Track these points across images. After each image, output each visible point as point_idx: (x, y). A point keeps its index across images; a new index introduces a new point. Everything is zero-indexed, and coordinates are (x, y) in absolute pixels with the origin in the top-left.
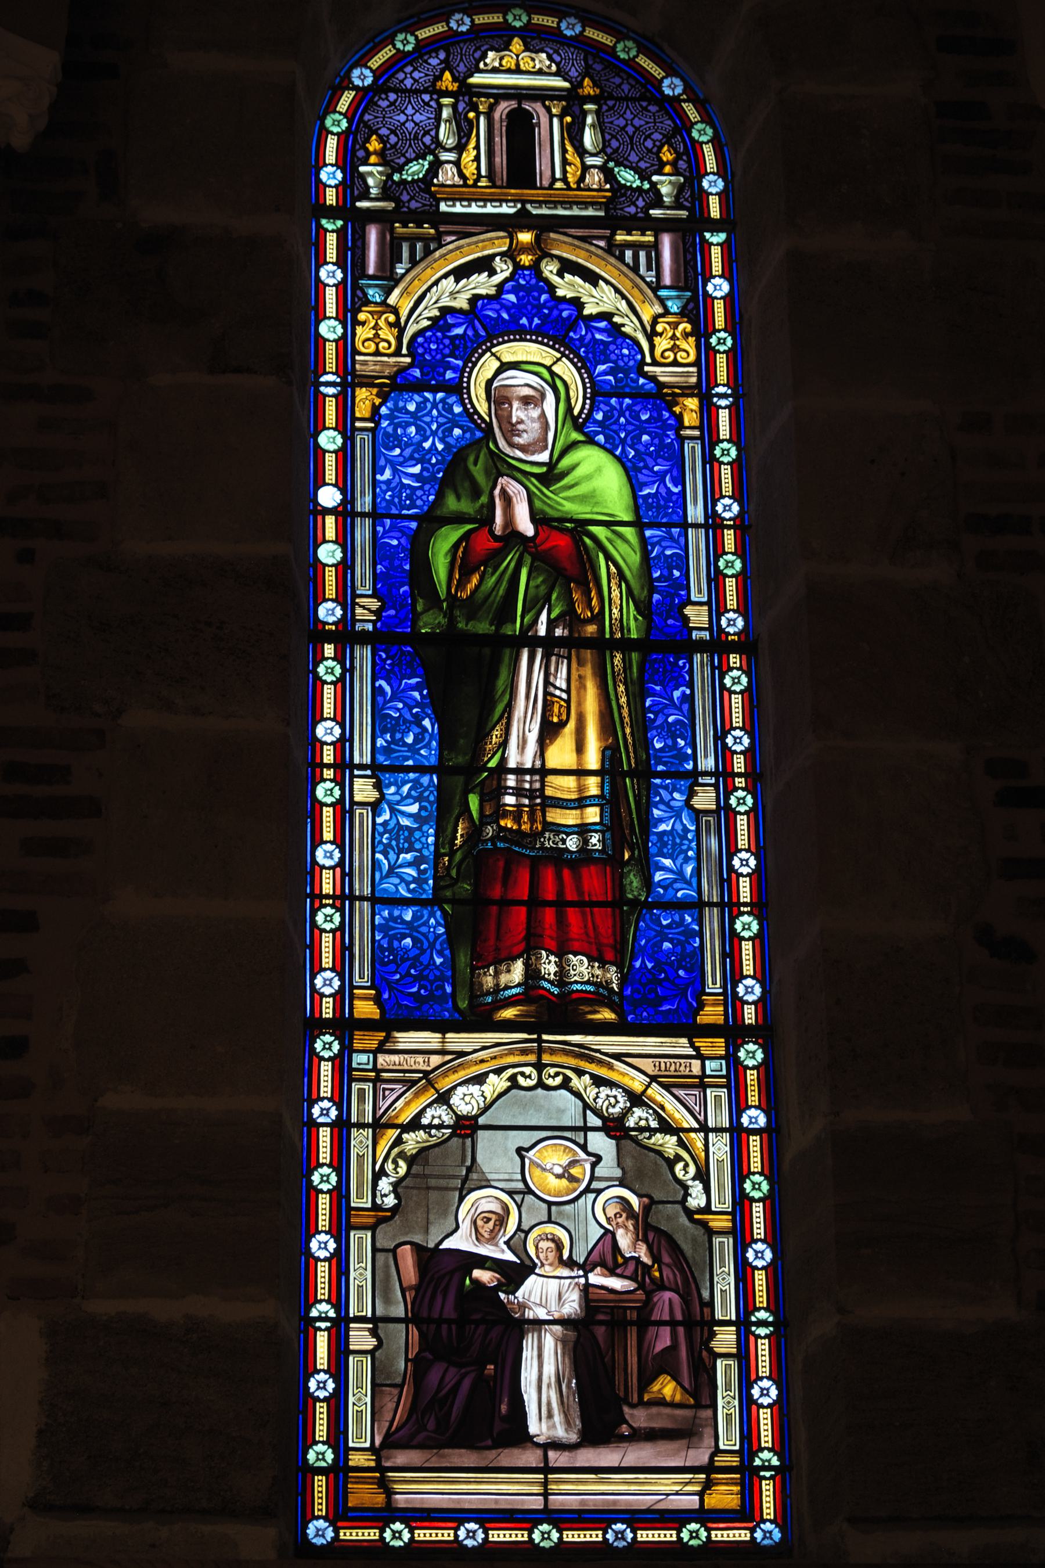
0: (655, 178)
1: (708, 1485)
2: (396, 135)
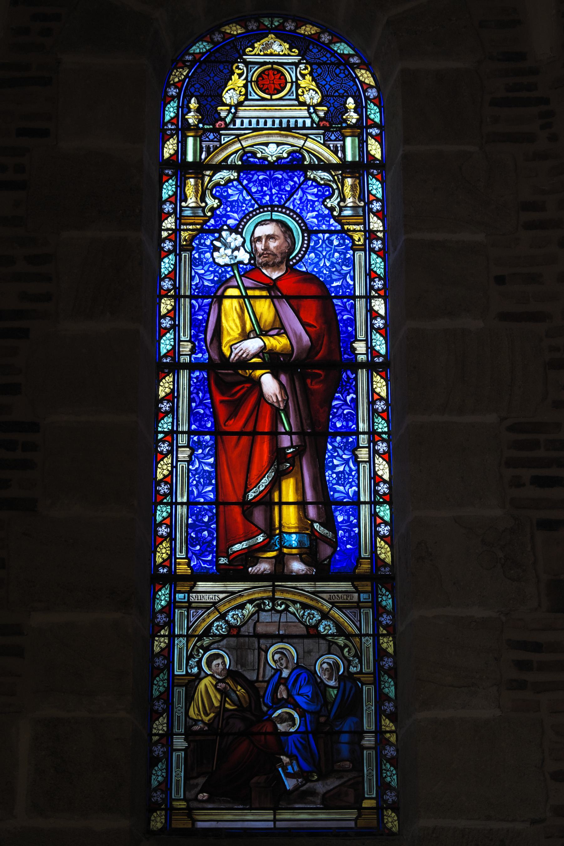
1: (359, 815)
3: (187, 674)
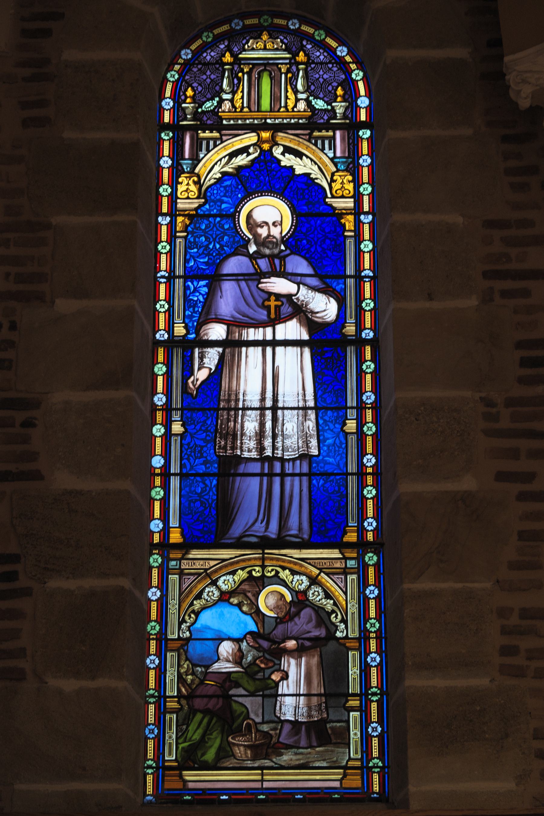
0: (334, 104)
1: (345, 775)
2: (201, 86)
3: (179, 638)
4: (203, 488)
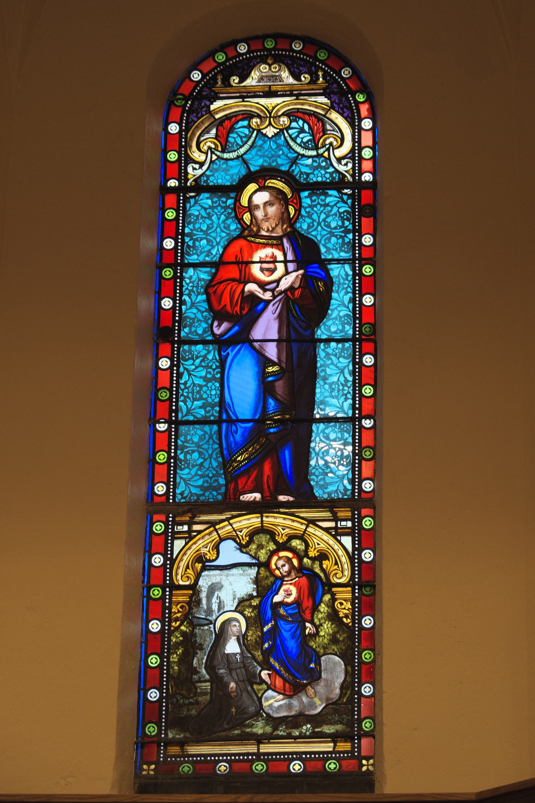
4: (202, 435)
